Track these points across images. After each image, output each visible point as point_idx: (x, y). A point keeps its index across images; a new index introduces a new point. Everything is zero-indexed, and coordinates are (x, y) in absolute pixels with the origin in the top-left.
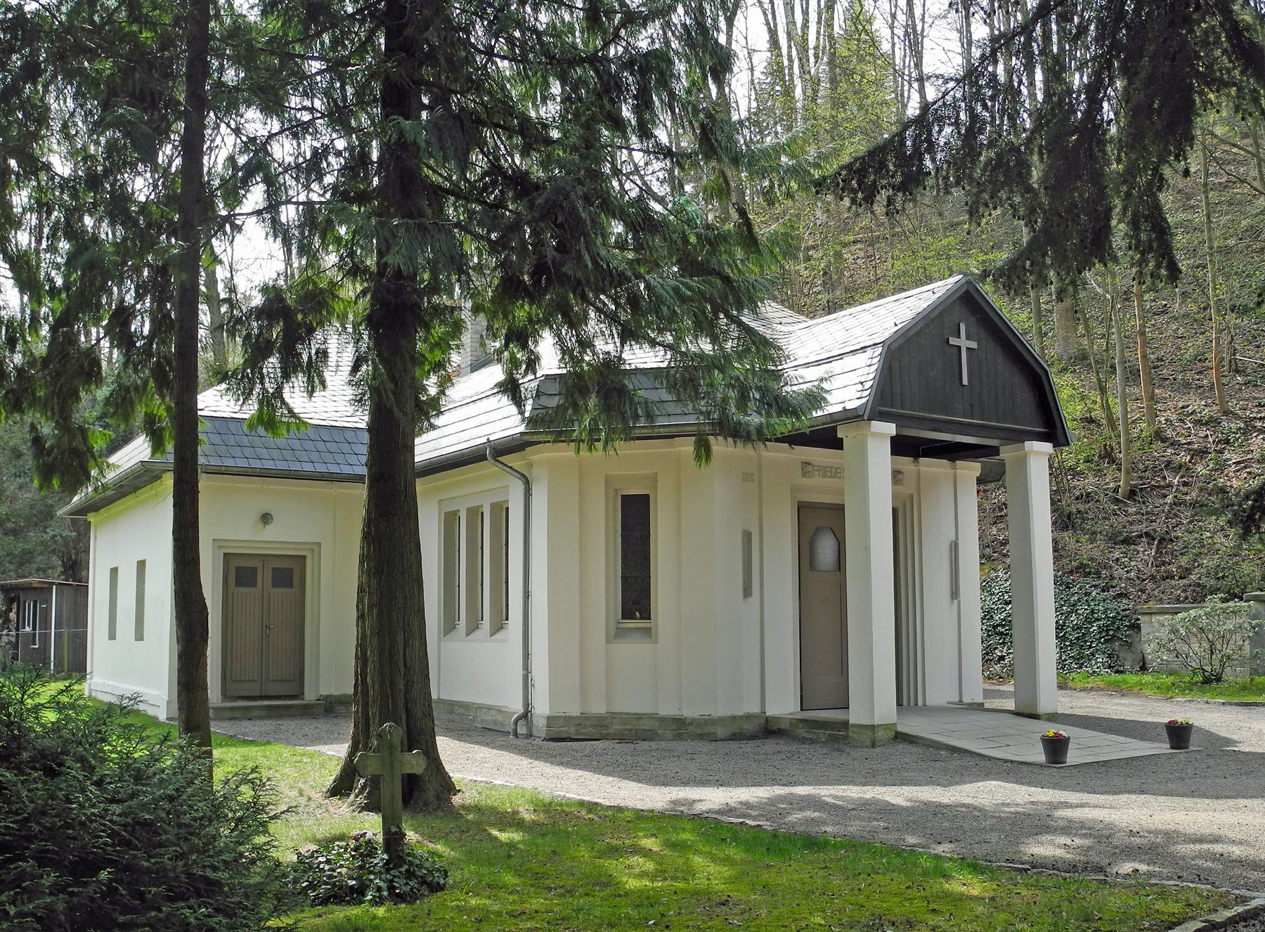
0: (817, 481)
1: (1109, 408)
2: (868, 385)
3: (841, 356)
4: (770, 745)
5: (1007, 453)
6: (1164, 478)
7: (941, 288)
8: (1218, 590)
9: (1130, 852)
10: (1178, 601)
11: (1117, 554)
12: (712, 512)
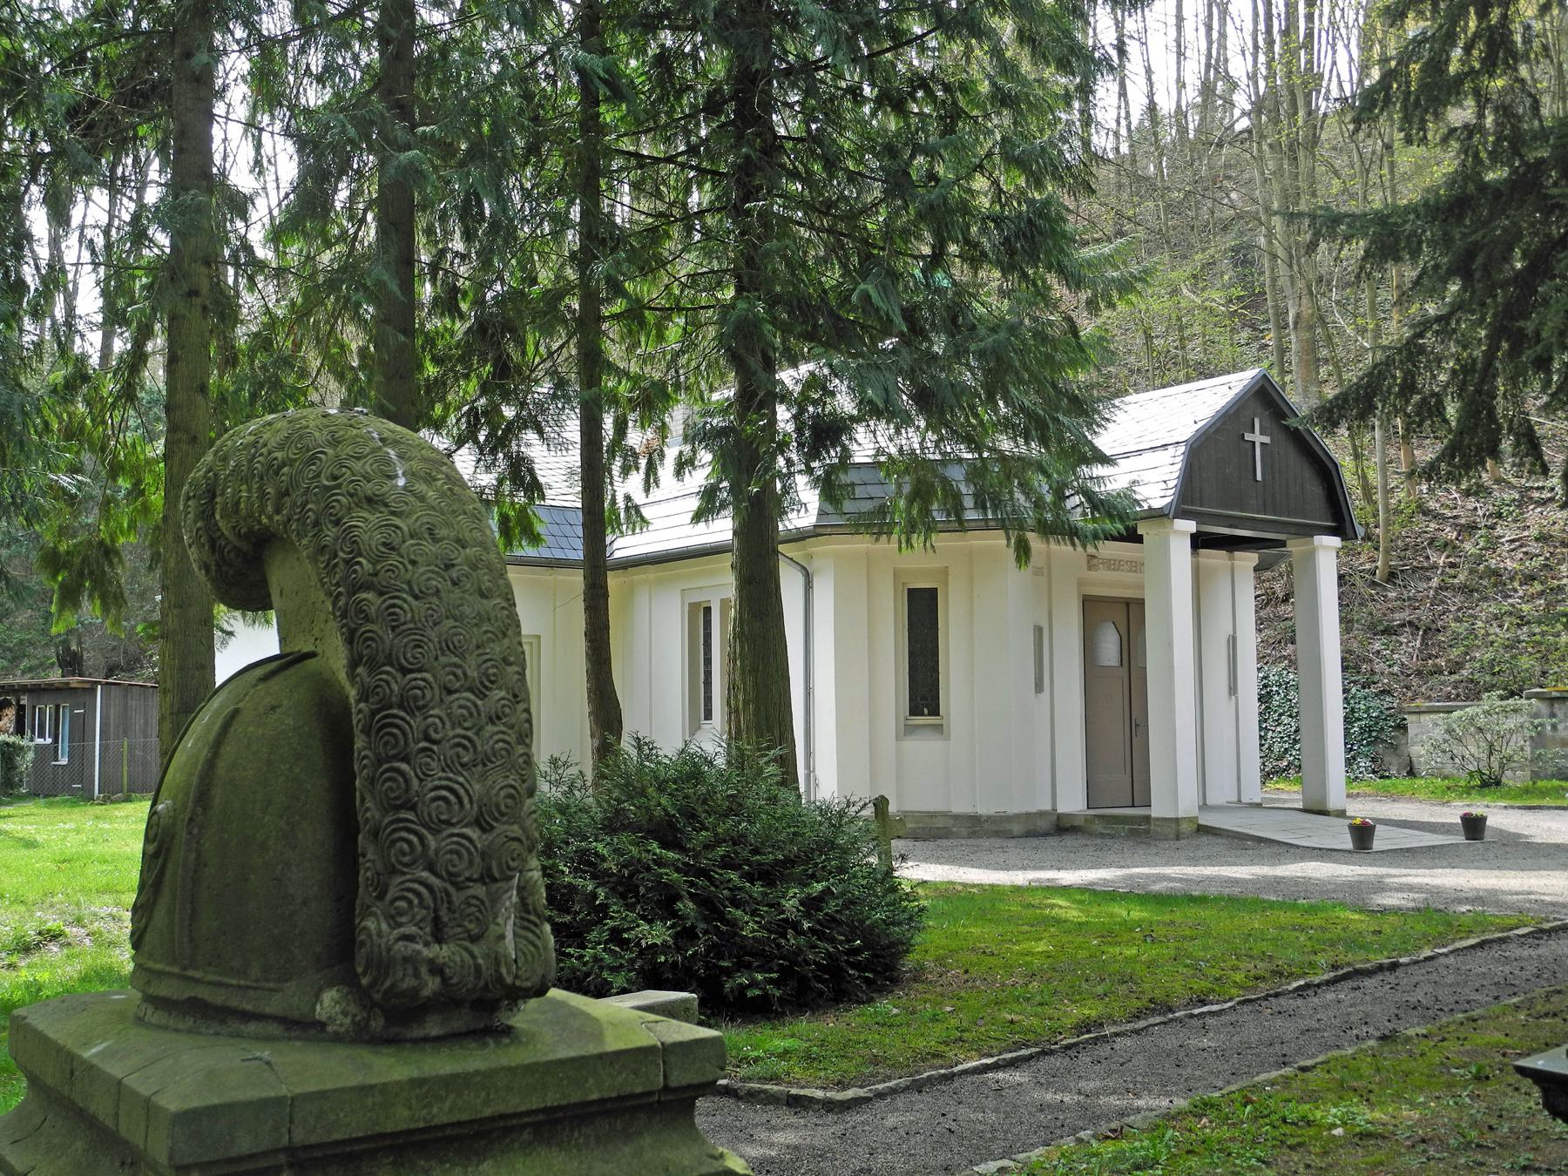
0: (1101, 574)
1: (1364, 477)
2: (1172, 484)
3: (1139, 452)
4: (1069, 841)
5: (1295, 547)
6: (1428, 558)
7: (1240, 381)
8: (1492, 687)
9: (1460, 901)
10: (1448, 698)
11: (1377, 646)
12: (1003, 610)
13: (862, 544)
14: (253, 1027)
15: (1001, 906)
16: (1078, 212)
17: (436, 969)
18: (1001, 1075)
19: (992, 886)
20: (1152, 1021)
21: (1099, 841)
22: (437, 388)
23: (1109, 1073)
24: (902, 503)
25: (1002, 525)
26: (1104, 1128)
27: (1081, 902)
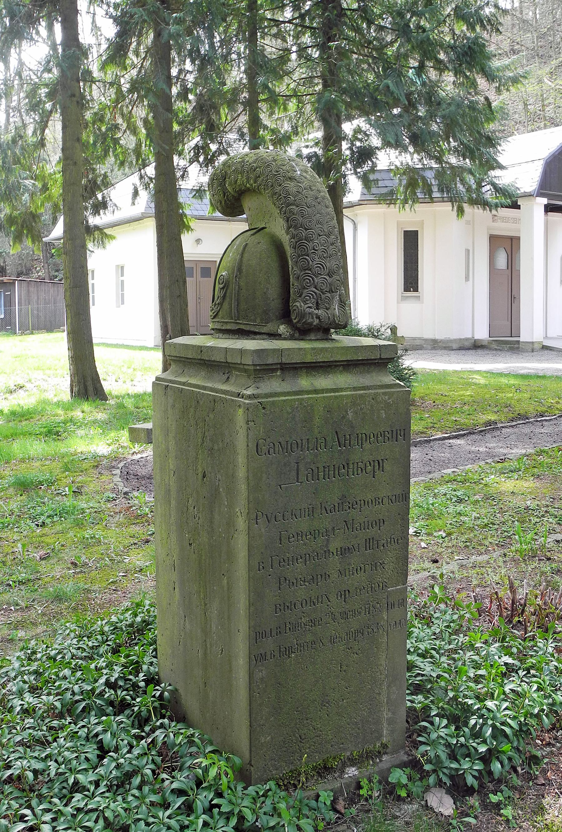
4: (480, 352)
12: (452, 240)
13: (382, 209)
14: (258, 337)
15: (449, 378)
16: (494, 43)
17: (318, 317)
18: (451, 441)
19: (444, 370)
20: (519, 422)
21: (494, 352)
22: (181, 137)
23: (500, 441)
24: (401, 189)
25: (451, 200)
26: (497, 459)
27: (485, 377)
